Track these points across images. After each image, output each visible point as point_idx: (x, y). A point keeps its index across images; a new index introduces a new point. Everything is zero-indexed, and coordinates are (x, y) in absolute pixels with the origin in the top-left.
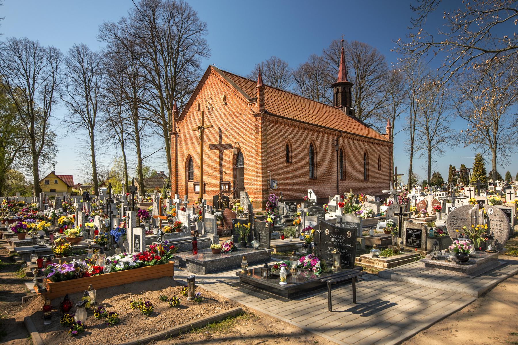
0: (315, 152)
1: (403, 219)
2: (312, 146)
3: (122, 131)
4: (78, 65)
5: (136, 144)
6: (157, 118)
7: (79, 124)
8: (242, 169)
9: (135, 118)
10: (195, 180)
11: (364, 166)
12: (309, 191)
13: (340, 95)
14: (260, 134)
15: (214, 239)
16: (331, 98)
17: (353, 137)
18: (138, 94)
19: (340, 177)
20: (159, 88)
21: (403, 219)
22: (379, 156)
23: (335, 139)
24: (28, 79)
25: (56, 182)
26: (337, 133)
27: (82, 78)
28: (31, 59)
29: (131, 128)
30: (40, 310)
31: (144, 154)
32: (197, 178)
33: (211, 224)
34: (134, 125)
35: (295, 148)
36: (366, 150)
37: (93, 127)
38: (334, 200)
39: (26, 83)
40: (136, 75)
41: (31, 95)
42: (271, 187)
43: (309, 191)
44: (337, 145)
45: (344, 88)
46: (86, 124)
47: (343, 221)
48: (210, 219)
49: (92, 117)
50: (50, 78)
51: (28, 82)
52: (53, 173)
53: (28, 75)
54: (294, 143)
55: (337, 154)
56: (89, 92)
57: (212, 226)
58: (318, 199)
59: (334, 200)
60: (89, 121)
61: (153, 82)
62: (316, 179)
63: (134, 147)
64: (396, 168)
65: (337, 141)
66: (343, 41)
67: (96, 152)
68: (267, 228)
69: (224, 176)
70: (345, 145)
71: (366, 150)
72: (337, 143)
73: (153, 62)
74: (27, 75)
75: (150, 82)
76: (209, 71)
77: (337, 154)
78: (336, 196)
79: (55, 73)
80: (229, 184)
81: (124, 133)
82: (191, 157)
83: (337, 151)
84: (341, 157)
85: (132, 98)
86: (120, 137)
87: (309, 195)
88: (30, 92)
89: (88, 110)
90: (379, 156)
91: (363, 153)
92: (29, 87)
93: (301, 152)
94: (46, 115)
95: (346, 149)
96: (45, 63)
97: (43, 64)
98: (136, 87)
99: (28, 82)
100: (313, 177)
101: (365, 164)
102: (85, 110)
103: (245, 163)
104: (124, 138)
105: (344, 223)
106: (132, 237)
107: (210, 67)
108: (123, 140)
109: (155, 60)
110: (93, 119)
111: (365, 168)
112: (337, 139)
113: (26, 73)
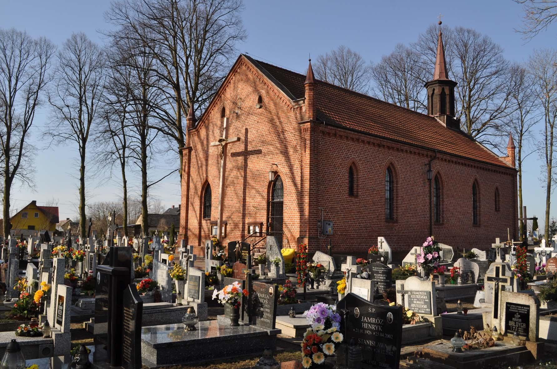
0: (395, 181)
1: (500, 287)
2: (391, 169)
3: (124, 147)
4: (73, 57)
5: (140, 164)
6: (173, 129)
7: (67, 136)
8: (281, 203)
9: (143, 128)
10: (212, 219)
11: (474, 204)
12: (380, 239)
13: (437, 100)
14: (308, 151)
15: (198, 308)
16: (426, 103)
18: (149, 95)
19: (434, 219)
20: (177, 87)
21: (500, 287)
22: (497, 189)
23: (427, 162)
24: (10, 77)
25: (36, 215)
26: (430, 153)
27: (78, 76)
28: (17, 52)
29: (134, 141)
30: (443, 358)
31: (150, 178)
32: (215, 213)
33: (197, 284)
34: (140, 137)
35: (362, 174)
36: (476, 180)
37: (84, 140)
38: (412, 254)
39: (7, 83)
40: (146, 71)
41: (11, 97)
42: (323, 232)
43: (380, 239)
44: (430, 171)
45: (443, 89)
46: (75, 135)
47: (406, 289)
48: (196, 277)
49: (86, 125)
50: (37, 75)
51: (10, 81)
52: (34, 203)
53: (11, 73)
54: (360, 167)
55: (430, 185)
56: (84, 93)
57: (197, 289)
58: (393, 252)
59: (412, 254)
60: (81, 131)
61: (170, 81)
62: (397, 222)
63: (139, 169)
64: (525, 207)
65: (429, 164)
66: (440, 23)
67: (86, 174)
68: (271, 294)
69: (242, 209)
70: (442, 172)
71: (476, 180)
72: (430, 167)
73: (172, 52)
74: (9, 73)
75: (165, 78)
76: (240, 60)
77: (430, 185)
78: (415, 248)
79: (43, 68)
80: (261, 224)
81: (126, 149)
82: (209, 184)
83: (430, 180)
84: (437, 189)
85: (140, 99)
86: (120, 155)
87: (379, 244)
88: (10, 93)
89: (80, 117)
90: (497, 189)
91: (471, 184)
92: (10, 87)
93: (372, 179)
94: (26, 124)
95: (444, 178)
96: (33, 56)
97: (31, 58)
98: (145, 85)
99: (10, 81)
100: (391, 218)
101: (475, 201)
102: (77, 116)
103: (285, 195)
104: (126, 155)
105: (407, 292)
106: (56, 299)
107: (241, 56)
108: (124, 157)
109: (174, 50)
110: (86, 128)
111: (475, 208)
112: (430, 162)
113: (9, 70)
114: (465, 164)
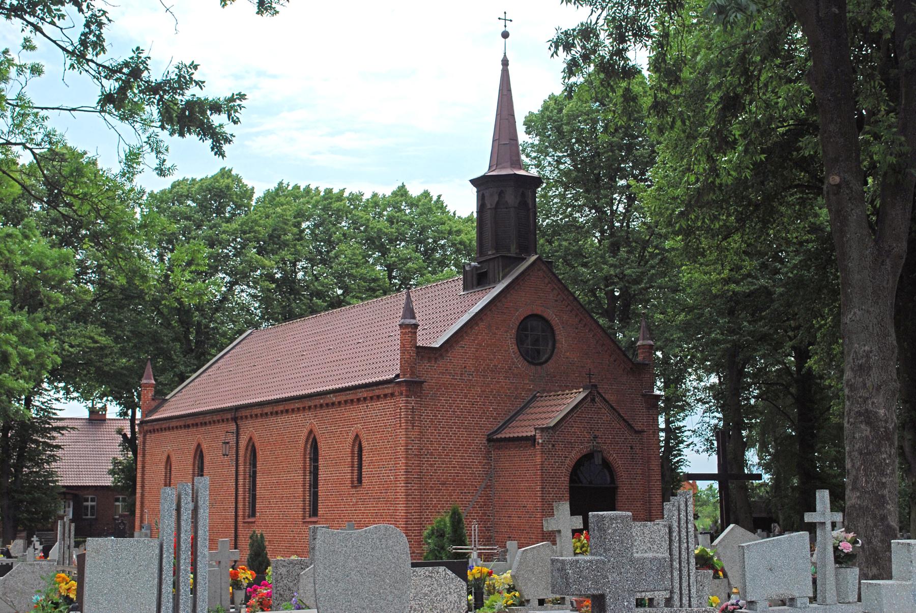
17: (267, 409)
64: (197, 490)
114: (287, 411)
